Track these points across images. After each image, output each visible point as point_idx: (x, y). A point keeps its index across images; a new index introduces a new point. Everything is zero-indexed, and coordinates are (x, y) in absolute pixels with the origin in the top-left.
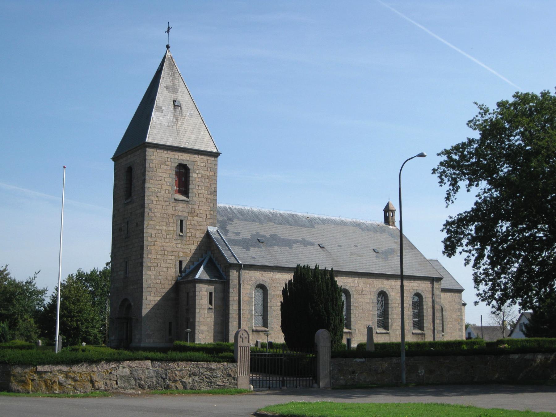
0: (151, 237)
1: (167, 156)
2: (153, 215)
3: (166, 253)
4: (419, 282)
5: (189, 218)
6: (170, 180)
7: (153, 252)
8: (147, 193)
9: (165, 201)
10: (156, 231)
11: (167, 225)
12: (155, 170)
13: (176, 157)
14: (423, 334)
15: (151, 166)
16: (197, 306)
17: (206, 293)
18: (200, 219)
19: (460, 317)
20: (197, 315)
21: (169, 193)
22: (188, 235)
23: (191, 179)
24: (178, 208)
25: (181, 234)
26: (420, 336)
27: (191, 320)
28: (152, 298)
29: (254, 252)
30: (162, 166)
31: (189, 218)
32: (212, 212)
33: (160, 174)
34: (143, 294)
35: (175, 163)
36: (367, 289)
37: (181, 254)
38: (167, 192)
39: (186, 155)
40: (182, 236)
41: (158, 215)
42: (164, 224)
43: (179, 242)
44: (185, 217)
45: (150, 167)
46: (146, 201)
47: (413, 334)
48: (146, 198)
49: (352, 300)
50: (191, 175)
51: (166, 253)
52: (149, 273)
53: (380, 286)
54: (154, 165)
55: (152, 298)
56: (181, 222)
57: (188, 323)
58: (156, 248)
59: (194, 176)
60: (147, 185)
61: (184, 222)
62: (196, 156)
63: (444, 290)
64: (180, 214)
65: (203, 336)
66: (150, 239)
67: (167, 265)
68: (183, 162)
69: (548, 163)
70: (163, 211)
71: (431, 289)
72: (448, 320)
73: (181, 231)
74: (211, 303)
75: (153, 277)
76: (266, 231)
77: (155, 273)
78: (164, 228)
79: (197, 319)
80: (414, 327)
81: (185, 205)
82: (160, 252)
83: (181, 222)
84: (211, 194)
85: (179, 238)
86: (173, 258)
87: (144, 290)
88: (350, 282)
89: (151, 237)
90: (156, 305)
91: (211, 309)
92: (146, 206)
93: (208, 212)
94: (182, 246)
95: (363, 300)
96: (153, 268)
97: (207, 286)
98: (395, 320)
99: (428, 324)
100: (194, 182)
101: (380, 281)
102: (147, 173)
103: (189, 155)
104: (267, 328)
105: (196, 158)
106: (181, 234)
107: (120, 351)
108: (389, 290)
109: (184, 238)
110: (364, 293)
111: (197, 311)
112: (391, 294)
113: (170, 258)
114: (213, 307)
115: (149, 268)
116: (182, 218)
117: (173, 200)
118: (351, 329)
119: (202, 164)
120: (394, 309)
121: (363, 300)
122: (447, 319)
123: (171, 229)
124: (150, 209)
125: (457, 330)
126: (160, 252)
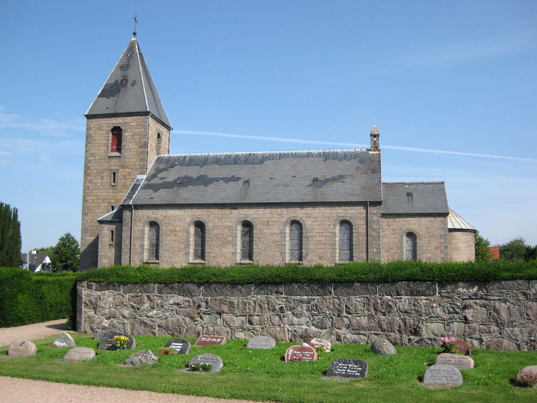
1: (104, 122)
2: (91, 172)
3: (101, 201)
4: (347, 208)
5: (120, 170)
7: (90, 201)
9: (101, 159)
10: (92, 184)
12: (93, 135)
13: (111, 122)
17: (107, 232)
18: (131, 170)
20: (99, 251)
22: (119, 184)
23: (123, 138)
24: (112, 163)
25: (113, 184)
28: (88, 238)
29: (162, 192)
31: (120, 170)
32: (141, 163)
33: (97, 138)
35: (110, 127)
37: (113, 201)
38: (102, 151)
39: (120, 118)
40: (113, 186)
41: (94, 171)
42: (100, 178)
43: (111, 191)
44: (117, 170)
49: (255, 231)
51: (101, 201)
55: (88, 238)
58: (93, 198)
59: (127, 135)
61: (116, 174)
62: (128, 118)
63: (384, 215)
64: (113, 168)
67: (101, 211)
68: (116, 125)
71: (365, 215)
72: (424, 248)
73: (114, 181)
74: (112, 240)
75: (89, 221)
76: (193, 172)
77: (91, 218)
78: (99, 181)
79: (99, 254)
81: (117, 160)
82: (95, 201)
83: (114, 174)
86: (106, 204)
88: (253, 213)
90: (91, 243)
91: (112, 245)
94: (114, 194)
96: (89, 214)
97: (110, 226)
99: (373, 250)
101: (292, 210)
103: (122, 118)
104: (158, 260)
105: (128, 119)
106: (113, 184)
108: (304, 219)
109: (116, 188)
110: (270, 223)
112: (306, 223)
113: (104, 204)
114: (114, 243)
116: (114, 171)
117: (107, 158)
118: (252, 261)
119: (133, 124)
120: (311, 239)
121: (269, 231)
122: (422, 246)
123: (105, 181)
126: (95, 201)
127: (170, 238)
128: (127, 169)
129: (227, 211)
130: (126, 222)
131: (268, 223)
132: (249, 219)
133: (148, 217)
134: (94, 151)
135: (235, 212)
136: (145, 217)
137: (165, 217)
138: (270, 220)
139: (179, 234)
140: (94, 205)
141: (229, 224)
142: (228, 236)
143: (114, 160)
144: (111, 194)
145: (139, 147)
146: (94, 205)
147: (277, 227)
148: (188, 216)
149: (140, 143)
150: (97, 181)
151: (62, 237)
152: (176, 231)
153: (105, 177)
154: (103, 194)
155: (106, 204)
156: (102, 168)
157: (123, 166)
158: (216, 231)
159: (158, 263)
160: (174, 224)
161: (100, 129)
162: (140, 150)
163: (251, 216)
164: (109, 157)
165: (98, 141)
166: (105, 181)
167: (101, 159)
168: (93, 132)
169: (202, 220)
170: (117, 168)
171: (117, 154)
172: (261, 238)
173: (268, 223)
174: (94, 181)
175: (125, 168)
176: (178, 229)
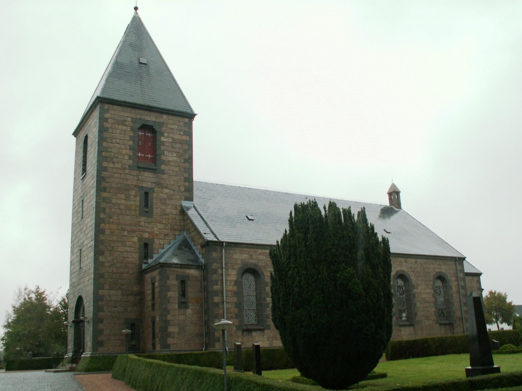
18: (172, 192)
51: (126, 233)
56: (147, 194)
61: (150, 195)
64: (144, 185)
83: (147, 194)
145: (182, 160)
146: (115, 238)
157: (159, 185)
161: (123, 122)
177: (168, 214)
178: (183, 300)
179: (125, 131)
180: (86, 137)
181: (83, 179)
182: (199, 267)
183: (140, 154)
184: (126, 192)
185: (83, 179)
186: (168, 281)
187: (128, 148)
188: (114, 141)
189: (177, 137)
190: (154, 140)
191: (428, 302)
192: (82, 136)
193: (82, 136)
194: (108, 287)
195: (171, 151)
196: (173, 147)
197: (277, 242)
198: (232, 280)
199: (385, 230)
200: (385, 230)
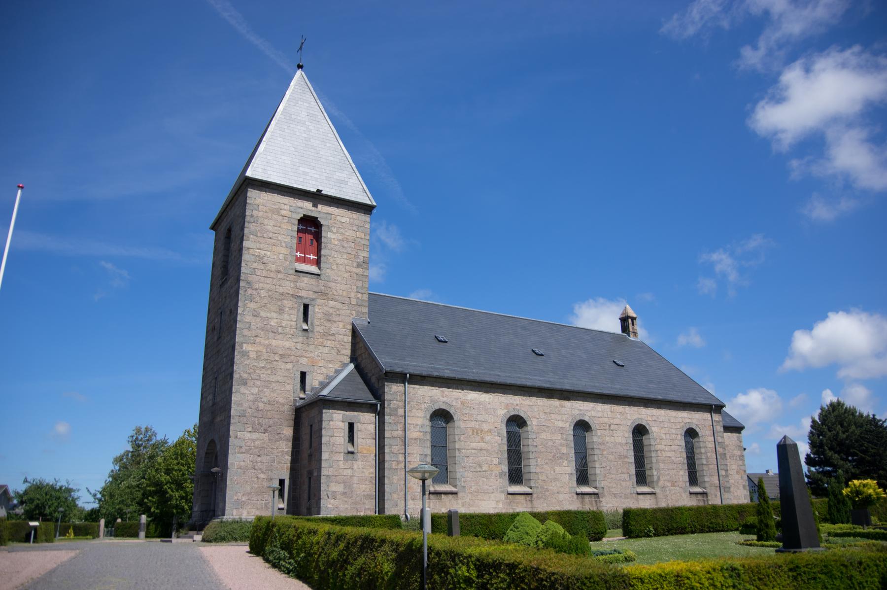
0: (249, 329)
5: (319, 301)
6: (288, 239)
8: (246, 257)
9: (279, 272)
10: (258, 319)
11: (281, 310)
12: (260, 220)
14: (704, 494)
15: (255, 215)
16: (324, 448)
17: (341, 424)
18: (339, 306)
19: (742, 468)
20: (324, 464)
21: (285, 259)
22: (317, 329)
25: (305, 327)
26: (700, 497)
27: (315, 474)
30: (275, 216)
32: (360, 296)
33: (269, 228)
34: (231, 428)
36: (616, 421)
38: (281, 257)
40: (305, 330)
43: (300, 339)
44: (313, 300)
45: (252, 216)
46: (243, 270)
47: (691, 493)
48: (243, 264)
50: (324, 234)
51: (277, 358)
52: (243, 389)
53: (635, 417)
54: (261, 214)
56: (306, 307)
57: (310, 478)
60: (246, 244)
61: (310, 308)
64: (303, 294)
65: (336, 502)
66: (246, 332)
69: (15, 506)
70: (273, 288)
75: (251, 398)
80: (98, 536)
81: (313, 281)
82: (265, 356)
83: (306, 307)
84: (359, 266)
85: (300, 333)
87: (232, 421)
89: (249, 329)
92: (242, 277)
93: (353, 295)
95: (612, 439)
96: (250, 383)
98: (662, 471)
99: (709, 478)
100: (329, 246)
102: (246, 225)
107: (866, 481)
109: (311, 335)
110: (612, 427)
111: (325, 456)
112: (654, 429)
115: (244, 383)
116: (307, 302)
117: (293, 272)
124: (248, 283)
125: (741, 488)
126: (265, 356)
127: (473, 445)
128: (332, 303)
129: (556, 403)
130: (392, 406)
131: (610, 426)
132: (586, 419)
133: (432, 401)
134: (263, 252)
135: (568, 404)
136: (427, 400)
137: (462, 403)
138: (612, 421)
139: (487, 438)
140: (262, 364)
141: (561, 424)
142: (562, 445)
143: (306, 279)
144: (299, 346)
145: (355, 265)
146: (262, 364)
147: (622, 435)
148: (497, 407)
149: (356, 256)
150: (269, 315)
151: (843, 404)
152: (482, 431)
153: (287, 309)
154: (282, 343)
155: (289, 366)
156: (281, 290)
157: (323, 294)
158: (543, 436)
159: (456, 494)
160: (479, 418)
161: (277, 211)
162: (354, 270)
163: (589, 414)
164: (296, 271)
165: (271, 235)
166: (286, 316)
167: (279, 272)
168: (261, 214)
169: (522, 415)
170: (312, 295)
171: (314, 269)
172: (603, 450)
173: (610, 426)
174: (262, 314)
175: (328, 299)
176: (485, 427)
177: (334, 335)
178: (351, 449)
179: (281, 223)
180: (230, 230)
181: (222, 285)
182: (152, 494)
183: (299, 254)
184: (279, 303)
185: (222, 285)
186: (331, 423)
187: (284, 245)
188: (265, 235)
189: (349, 233)
190: (318, 236)
191: (673, 463)
192: (223, 227)
193: (223, 227)
194: (250, 429)
195: (340, 252)
196: (343, 247)
197: (785, 451)
198: (417, 425)
199: (303, 375)
200: (303, 375)
